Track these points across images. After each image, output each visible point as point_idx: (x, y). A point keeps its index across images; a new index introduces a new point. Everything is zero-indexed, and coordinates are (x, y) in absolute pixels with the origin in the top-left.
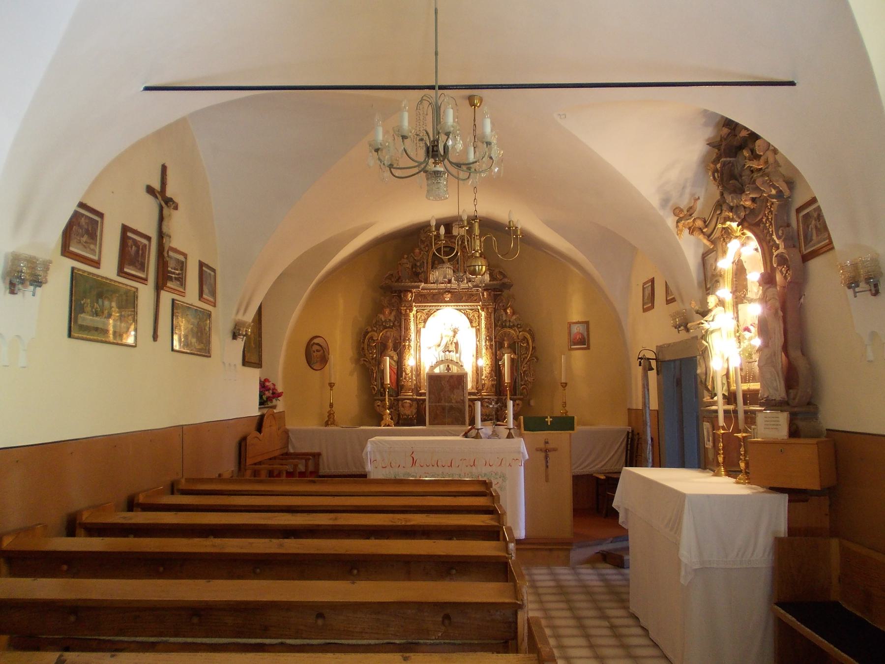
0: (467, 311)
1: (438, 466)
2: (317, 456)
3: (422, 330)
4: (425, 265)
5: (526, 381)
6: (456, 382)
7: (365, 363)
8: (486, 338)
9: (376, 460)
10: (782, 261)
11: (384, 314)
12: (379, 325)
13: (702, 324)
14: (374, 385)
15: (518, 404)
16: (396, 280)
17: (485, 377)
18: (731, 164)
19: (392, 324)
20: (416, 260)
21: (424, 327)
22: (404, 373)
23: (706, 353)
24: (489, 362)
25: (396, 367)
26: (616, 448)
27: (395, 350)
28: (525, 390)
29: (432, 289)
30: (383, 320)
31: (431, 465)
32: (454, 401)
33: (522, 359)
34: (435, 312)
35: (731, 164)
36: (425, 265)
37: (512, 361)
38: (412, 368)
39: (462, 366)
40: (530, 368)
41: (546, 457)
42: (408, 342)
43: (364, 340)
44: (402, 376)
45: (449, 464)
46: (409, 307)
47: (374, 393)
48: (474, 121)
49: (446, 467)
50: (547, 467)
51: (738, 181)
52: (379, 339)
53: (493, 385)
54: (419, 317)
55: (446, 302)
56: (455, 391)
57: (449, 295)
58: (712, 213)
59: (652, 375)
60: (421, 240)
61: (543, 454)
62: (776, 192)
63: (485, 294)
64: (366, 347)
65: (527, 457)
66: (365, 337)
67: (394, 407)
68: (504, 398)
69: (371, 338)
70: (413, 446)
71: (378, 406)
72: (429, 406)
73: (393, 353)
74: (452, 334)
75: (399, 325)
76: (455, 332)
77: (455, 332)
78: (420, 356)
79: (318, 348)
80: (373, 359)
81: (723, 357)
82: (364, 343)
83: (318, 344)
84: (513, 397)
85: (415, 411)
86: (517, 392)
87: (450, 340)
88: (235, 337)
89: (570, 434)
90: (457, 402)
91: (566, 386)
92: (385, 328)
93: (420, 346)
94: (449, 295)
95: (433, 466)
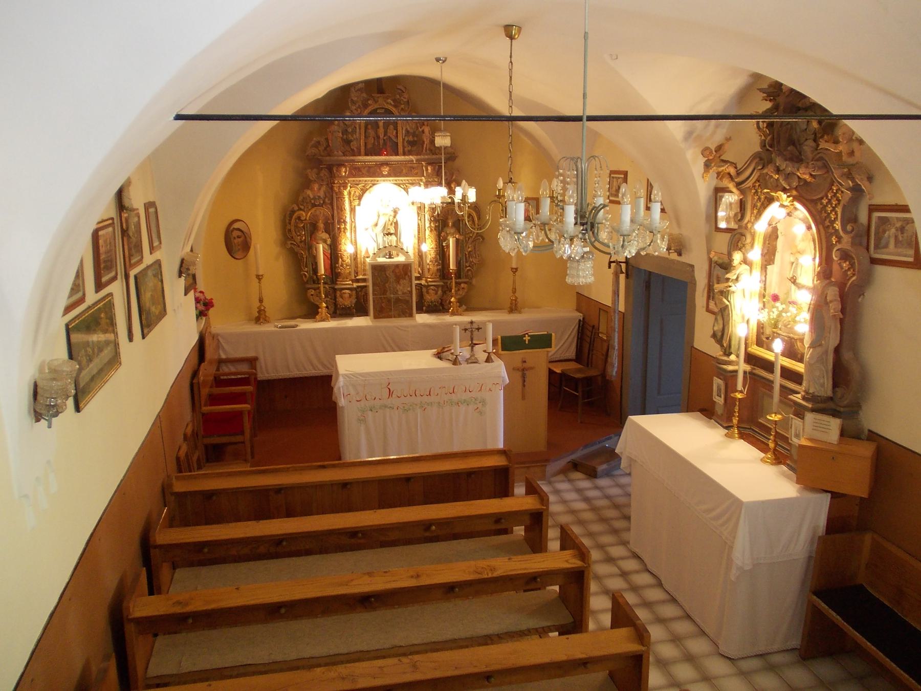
0: (406, 186)
1: (416, 395)
2: (252, 361)
3: (357, 208)
4: (358, 130)
5: (471, 262)
6: (402, 272)
7: (293, 246)
8: (431, 219)
9: (349, 394)
10: (845, 256)
11: (312, 190)
12: (307, 203)
13: (730, 287)
14: (305, 272)
15: (463, 288)
16: (323, 148)
17: (430, 262)
18: (789, 126)
19: (322, 202)
20: (346, 125)
21: (359, 205)
22: (340, 260)
23: (727, 312)
24: (433, 245)
25: (329, 252)
26: (566, 337)
27: (326, 232)
28: (470, 273)
29: (367, 162)
30: (312, 197)
31: (409, 396)
32: (400, 293)
33: (467, 239)
34: (371, 187)
35: (789, 126)
36: (358, 130)
37: (457, 242)
38: (351, 254)
39: (407, 252)
40: (475, 248)
41: (524, 377)
42: (343, 224)
43: (290, 220)
44: (338, 263)
45: (428, 393)
46: (343, 183)
47: (305, 280)
48: (511, 57)
49: (425, 396)
50: (524, 386)
51: (797, 149)
52: (308, 219)
53: (438, 270)
54: (352, 193)
55: (383, 176)
56: (402, 282)
57: (387, 169)
58: (749, 162)
59: (622, 277)
60: (352, 100)
61: (519, 374)
62: (853, 186)
63: (429, 168)
64: (293, 228)
65: (507, 381)
66: (291, 217)
67: (330, 295)
68: (449, 282)
69: (299, 218)
70: (390, 377)
71: (312, 295)
72: (373, 298)
73: (325, 236)
74: (392, 214)
75: (333, 201)
76: (395, 212)
77: (395, 212)
78: (355, 237)
79: (239, 233)
80: (301, 242)
81: (743, 317)
82: (290, 224)
83: (239, 230)
84: (457, 281)
85: (354, 301)
86: (462, 274)
87: (389, 220)
88: (180, 276)
89: (548, 351)
90: (403, 293)
91: (516, 272)
92: (314, 205)
93: (355, 227)
94: (387, 169)
95: (411, 396)
